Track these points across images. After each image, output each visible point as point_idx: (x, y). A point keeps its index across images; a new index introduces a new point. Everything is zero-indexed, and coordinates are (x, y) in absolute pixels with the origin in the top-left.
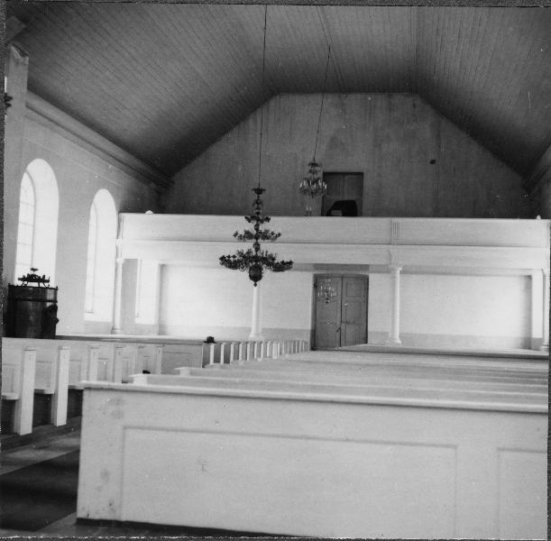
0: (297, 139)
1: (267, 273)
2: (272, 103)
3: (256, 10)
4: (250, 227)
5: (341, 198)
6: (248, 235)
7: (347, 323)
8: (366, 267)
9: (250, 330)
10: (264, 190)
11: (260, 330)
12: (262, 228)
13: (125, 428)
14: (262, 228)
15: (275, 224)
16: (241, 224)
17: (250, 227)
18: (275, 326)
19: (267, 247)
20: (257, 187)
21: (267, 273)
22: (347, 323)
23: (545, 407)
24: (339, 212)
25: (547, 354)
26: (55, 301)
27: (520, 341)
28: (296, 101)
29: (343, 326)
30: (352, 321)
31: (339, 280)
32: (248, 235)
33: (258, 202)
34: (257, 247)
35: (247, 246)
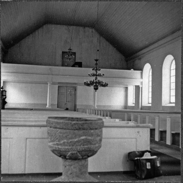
0: (57, 38)
1: (100, 88)
2: (44, 26)
3: (96, 3)
4: (94, 72)
5: (70, 59)
6: (94, 75)
7: (69, 102)
8: (75, 84)
9: (46, 104)
10: (98, 60)
11: (50, 105)
12: (99, 72)
13: (136, 138)
14: (99, 72)
15: (102, 71)
16: (91, 71)
17: (94, 72)
18: (26, 103)
19: (99, 78)
20: (96, 59)
21: (100, 88)
22: (69, 102)
23: (3, 128)
24: (77, 66)
25: (180, 111)
26: (6, 96)
27: (123, 107)
28: (52, 27)
29: (67, 103)
30: (70, 101)
31: (66, 88)
32: (94, 75)
33: (96, 64)
34: (96, 78)
35: (93, 79)
